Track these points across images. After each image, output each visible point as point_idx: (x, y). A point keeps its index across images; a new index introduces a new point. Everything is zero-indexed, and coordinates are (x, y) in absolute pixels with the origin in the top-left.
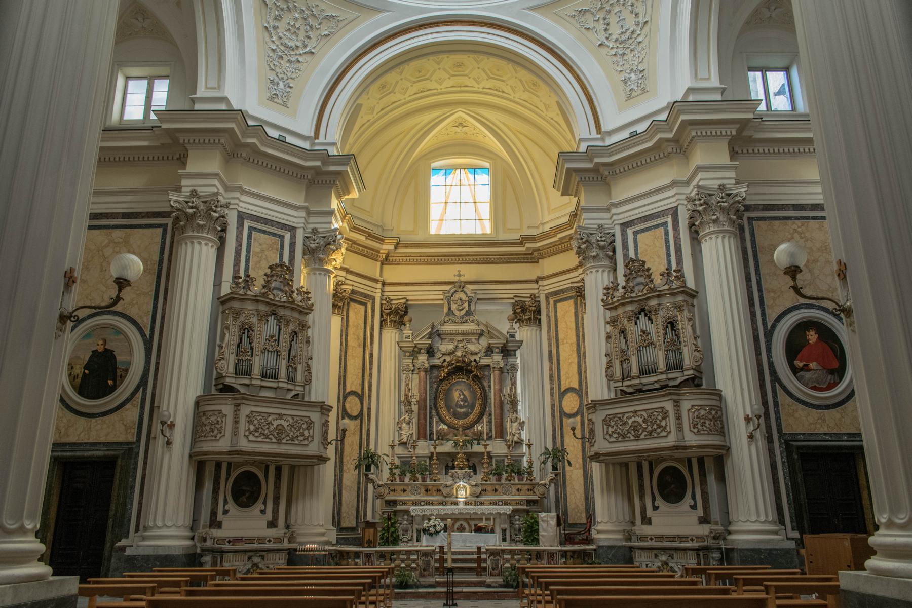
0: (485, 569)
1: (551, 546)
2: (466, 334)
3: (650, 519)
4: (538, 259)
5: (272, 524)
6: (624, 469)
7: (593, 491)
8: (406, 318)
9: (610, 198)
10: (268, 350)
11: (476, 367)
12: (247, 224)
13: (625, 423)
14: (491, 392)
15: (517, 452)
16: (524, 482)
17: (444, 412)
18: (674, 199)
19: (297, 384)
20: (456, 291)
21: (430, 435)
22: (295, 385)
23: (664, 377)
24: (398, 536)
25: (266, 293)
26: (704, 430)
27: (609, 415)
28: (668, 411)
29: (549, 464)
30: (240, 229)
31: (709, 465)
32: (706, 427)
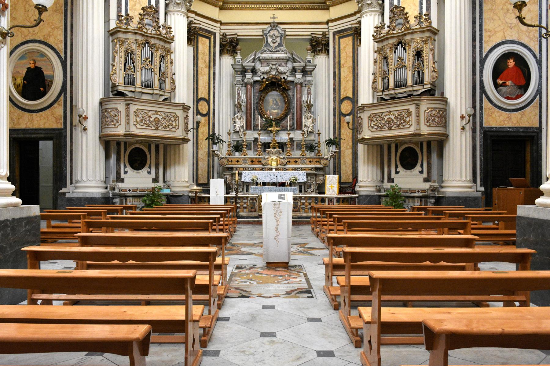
3: (393, 179)
7: (357, 163)
20: (272, 29)
22: (165, 92)
23: (410, 89)
25: (141, 27)
26: (433, 124)
27: (373, 114)
31: (434, 146)
32: (435, 122)
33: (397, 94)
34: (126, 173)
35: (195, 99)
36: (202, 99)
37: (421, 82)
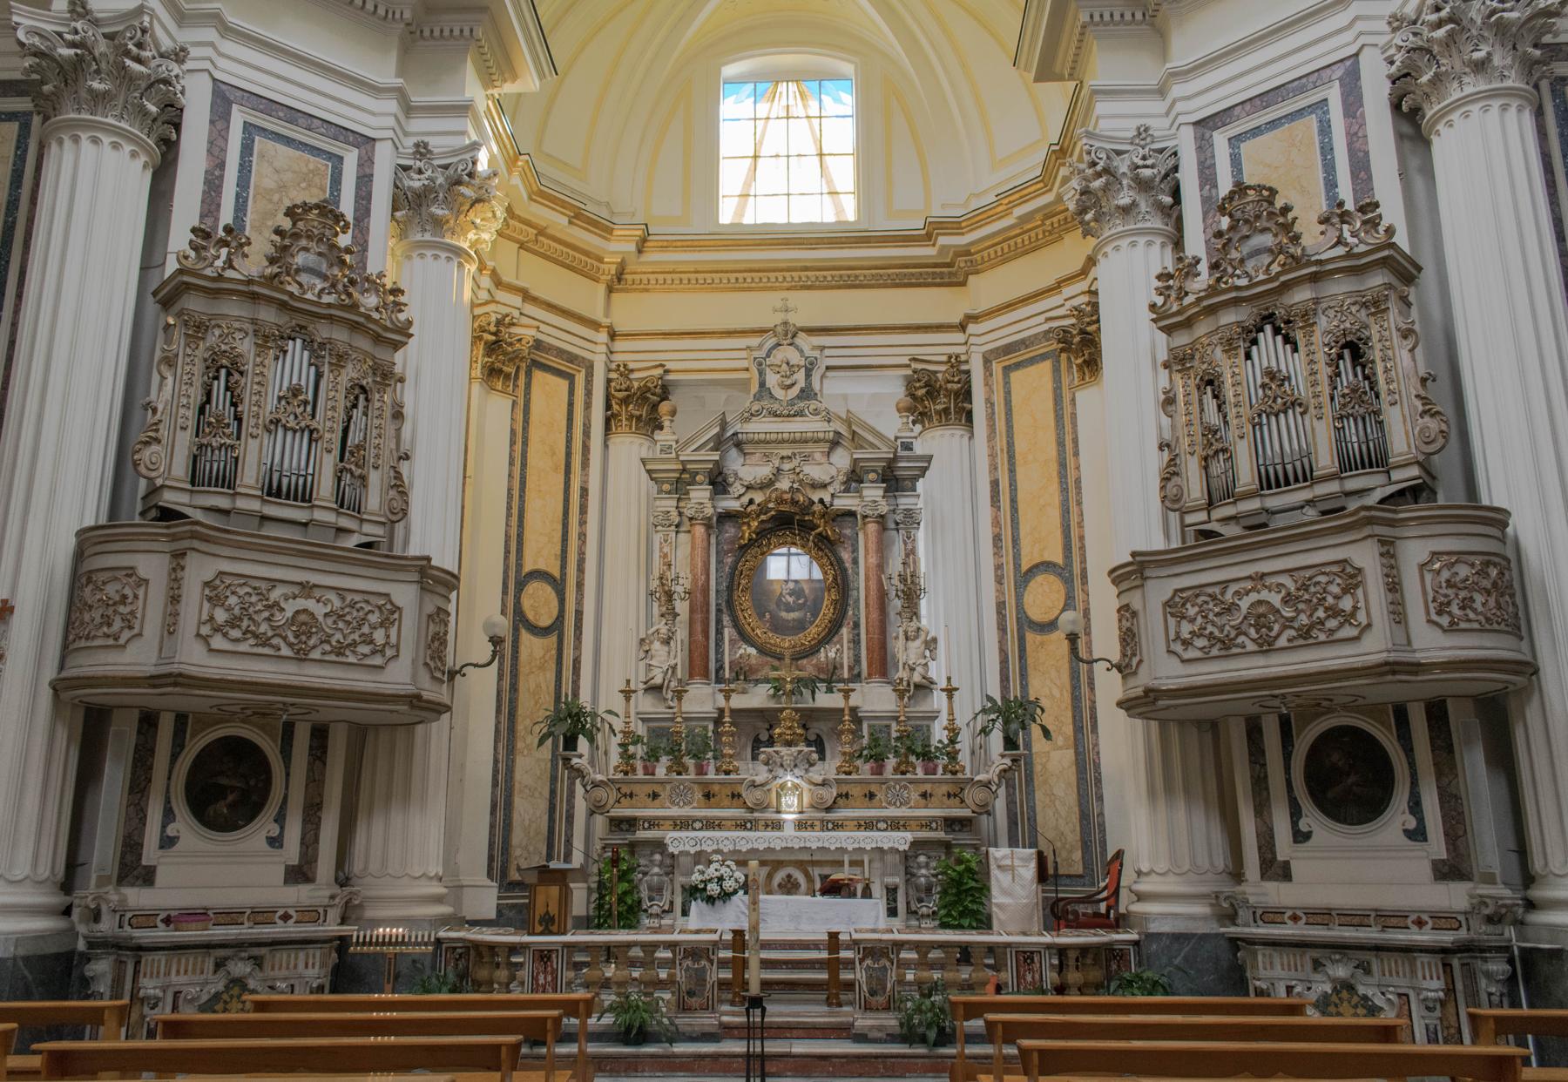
0: (850, 986)
1: (1025, 934)
2: (794, 441)
3: (1286, 865)
4: (967, 275)
5: (299, 874)
6: (1208, 737)
7: (1100, 798)
8: (664, 407)
9: (1164, 54)
10: (284, 426)
11: (823, 516)
12: (238, 118)
13: (1229, 610)
14: (858, 574)
15: (924, 707)
16: (938, 776)
17: (750, 619)
18: (1348, 36)
19: (365, 517)
20: (779, 345)
21: (717, 672)
22: (362, 521)
23: (1333, 487)
24: (640, 902)
25: (277, 275)
26: (1469, 621)
27: (1182, 590)
28: (1360, 570)
29: (996, 738)
30: (220, 125)
31: (1461, 719)
32: (1474, 610)
33: (1271, 513)
34: (167, 842)
35: (512, 574)
36: (537, 575)
37: (1376, 459)
